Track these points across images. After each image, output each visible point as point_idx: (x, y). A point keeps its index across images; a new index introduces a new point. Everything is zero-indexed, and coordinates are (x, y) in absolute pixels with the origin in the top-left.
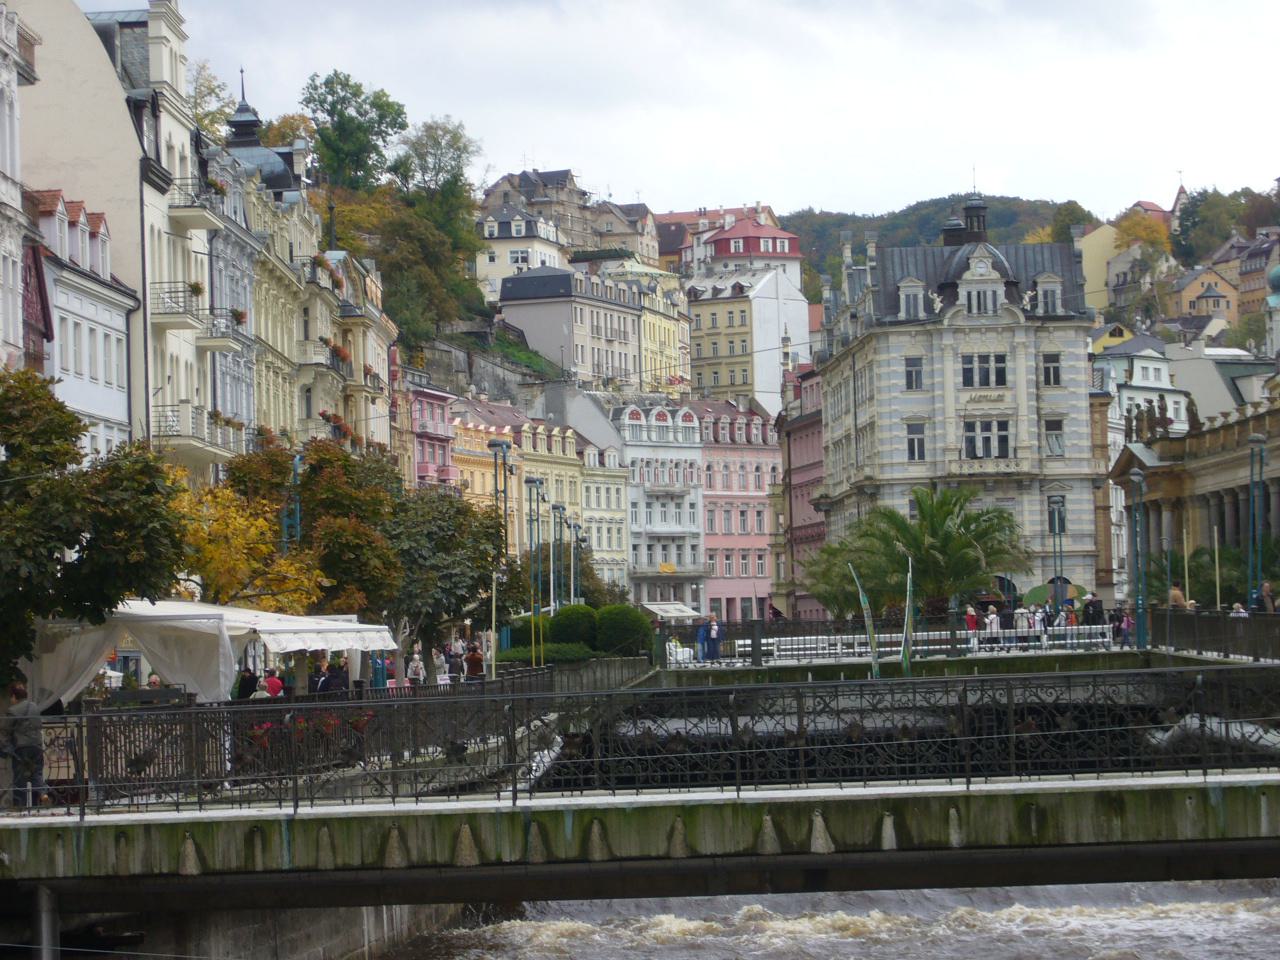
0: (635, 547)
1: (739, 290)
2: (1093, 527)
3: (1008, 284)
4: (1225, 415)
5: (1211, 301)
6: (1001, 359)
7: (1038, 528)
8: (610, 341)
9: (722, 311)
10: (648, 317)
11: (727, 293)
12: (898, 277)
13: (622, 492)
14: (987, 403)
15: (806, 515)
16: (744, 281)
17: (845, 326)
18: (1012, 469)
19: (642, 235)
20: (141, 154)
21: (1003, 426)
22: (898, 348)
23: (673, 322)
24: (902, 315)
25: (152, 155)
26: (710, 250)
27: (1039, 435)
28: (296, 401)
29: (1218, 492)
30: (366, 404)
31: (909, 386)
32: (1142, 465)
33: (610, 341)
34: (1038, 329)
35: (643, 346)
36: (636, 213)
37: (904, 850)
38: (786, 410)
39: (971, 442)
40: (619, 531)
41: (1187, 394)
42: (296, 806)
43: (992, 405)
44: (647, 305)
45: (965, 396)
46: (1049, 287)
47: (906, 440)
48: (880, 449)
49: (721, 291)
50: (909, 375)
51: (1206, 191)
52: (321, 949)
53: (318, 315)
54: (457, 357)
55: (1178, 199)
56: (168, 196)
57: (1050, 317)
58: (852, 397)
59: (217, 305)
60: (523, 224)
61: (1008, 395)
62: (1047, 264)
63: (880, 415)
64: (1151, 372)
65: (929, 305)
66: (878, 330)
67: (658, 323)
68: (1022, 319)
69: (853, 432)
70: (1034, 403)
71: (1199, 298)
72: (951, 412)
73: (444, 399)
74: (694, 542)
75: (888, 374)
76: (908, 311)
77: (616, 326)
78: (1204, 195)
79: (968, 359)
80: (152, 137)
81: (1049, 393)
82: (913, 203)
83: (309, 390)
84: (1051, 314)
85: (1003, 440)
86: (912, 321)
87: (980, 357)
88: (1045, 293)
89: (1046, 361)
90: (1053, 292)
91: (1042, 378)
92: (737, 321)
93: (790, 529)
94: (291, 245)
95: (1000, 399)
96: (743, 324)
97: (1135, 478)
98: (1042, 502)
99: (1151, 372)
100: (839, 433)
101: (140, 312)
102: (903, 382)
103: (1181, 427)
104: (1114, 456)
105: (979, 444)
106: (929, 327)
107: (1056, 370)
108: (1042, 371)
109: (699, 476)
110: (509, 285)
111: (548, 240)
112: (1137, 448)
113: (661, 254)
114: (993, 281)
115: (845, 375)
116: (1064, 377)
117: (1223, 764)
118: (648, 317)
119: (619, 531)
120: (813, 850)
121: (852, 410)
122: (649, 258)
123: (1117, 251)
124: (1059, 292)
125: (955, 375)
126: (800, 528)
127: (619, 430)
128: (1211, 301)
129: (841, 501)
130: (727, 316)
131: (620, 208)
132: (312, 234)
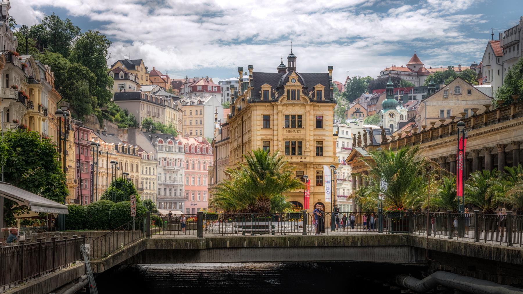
0: (159, 189)
1: (200, 103)
3: (303, 88)
5: (358, 114)
8: (153, 117)
9: (193, 109)
10: (167, 109)
14: (295, 134)
16: (202, 100)
18: (303, 160)
23: (176, 111)
24: (262, 99)
26: (190, 89)
30: (39, 121)
33: (153, 117)
34: (314, 106)
35: (165, 119)
44: (167, 105)
45: (285, 131)
53: (13, 78)
57: (320, 101)
60: (123, 74)
64: (345, 133)
65: (273, 94)
66: (253, 104)
67: (171, 112)
68: (309, 101)
69: (241, 144)
72: (280, 138)
73: (88, 132)
74: (181, 188)
77: (156, 111)
83: (8, 110)
86: (266, 101)
92: (199, 113)
96: (201, 114)
99: (345, 133)
106: (273, 103)
109: (183, 165)
110: (117, 95)
111: (132, 81)
112: (359, 150)
114: (298, 86)
115: (239, 123)
124: (323, 91)
127: (154, 146)
128: (358, 114)
130: (195, 111)
132: (13, 43)
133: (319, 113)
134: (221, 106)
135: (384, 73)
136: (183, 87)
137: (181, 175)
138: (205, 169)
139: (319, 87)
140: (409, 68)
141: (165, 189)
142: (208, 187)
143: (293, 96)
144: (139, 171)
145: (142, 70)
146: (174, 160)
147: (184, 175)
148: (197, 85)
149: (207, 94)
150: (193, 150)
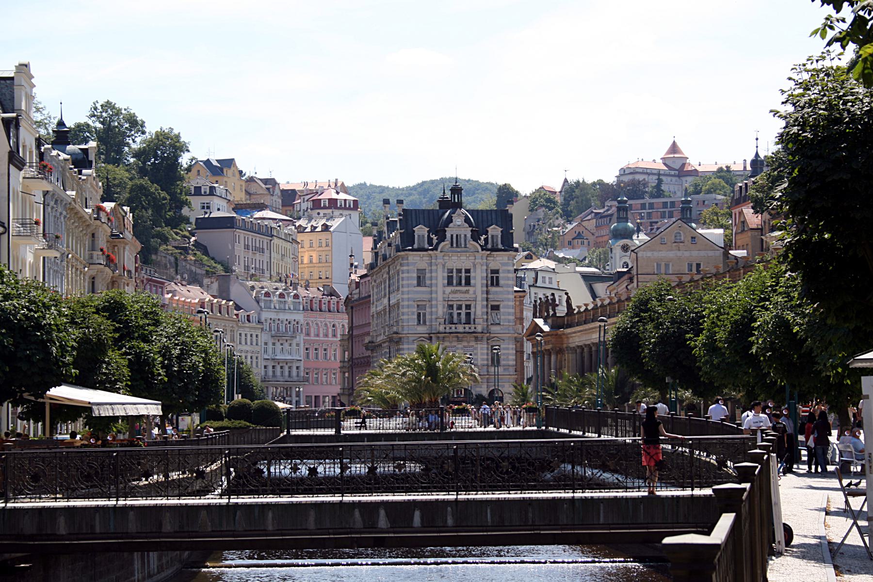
0: (265, 367)
1: (326, 228)
2: (514, 363)
4: (586, 305)
6: (468, 271)
7: (486, 362)
11: (319, 229)
12: (414, 225)
13: (259, 337)
14: (460, 295)
15: (360, 351)
16: (328, 223)
17: (385, 251)
19: (272, 195)
20: (9, 149)
21: (468, 307)
22: (416, 260)
23: (289, 243)
24: (416, 246)
25: (15, 150)
26: (310, 204)
27: (487, 313)
28: (86, 284)
29: (581, 346)
31: (419, 285)
32: (542, 331)
36: (271, 183)
37: (424, 527)
38: (351, 294)
39: (451, 315)
40: (257, 358)
41: (566, 294)
42: (117, 500)
43: (462, 295)
45: (449, 289)
46: (495, 233)
47: (416, 314)
48: (402, 317)
49: (316, 228)
50: (419, 278)
51: (578, 182)
52: (114, 577)
54: (170, 260)
55: (564, 185)
56: (22, 172)
57: (495, 249)
58: (387, 289)
59: (47, 232)
61: (471, 289)
62: (494, 221)
63: (403, 300)
69: (387, 307)
70: (485, 296)
71: (573, 239)
72: (440, 298)
75: (408, 277)
76: (419, 244)
78: (578, 183)
79: (451, 271)
80: (15, 140)
81: (493, 289)
82: (420, 182)
83: (93, 278)
84: (495, 247)
85: (468, 315)
87: (457, 269)
88: (492, 236)
89: (491, 273)
90: (497, 236)
91: (489, 282)
93: (351, 359)
94: (86, 199)
95: (467, 292)
97: (539, 338)
98: (488, 349)
100: (380, 308)
101: (7, 234)
102: (415, 282)
103: (562, 311)
104: (526, 324)
105: (455, 316)
107: (497, 277)
108: (489, 279)
112: (540, 322)
113: (282, 206)
116: (501, 282)
117: (583, 488)
118: (276, 241)
119: (257, 358)
120: (379, 526)
121: (388, 296)
122: (276, 208)
123: (530, 213)
125: (443, 279)
126: (357, 359)
129: (380, 345)
131: (261, 180)
133: (493, 266)
134: (360, 232)
135: (624, 171)
136: (299, 201)
137: (298, 345)
138: (334, 336)
139: (495, 231)
140: (665, 164)
141: (274, 367)
142: (339, 365)
143: (456, 242)
144: (235, 340)
145: (234, 175)
146: (287, 323)
147: (302, 345)
148: (320, 198)
149: (337, 212)
150: (316, 306)
